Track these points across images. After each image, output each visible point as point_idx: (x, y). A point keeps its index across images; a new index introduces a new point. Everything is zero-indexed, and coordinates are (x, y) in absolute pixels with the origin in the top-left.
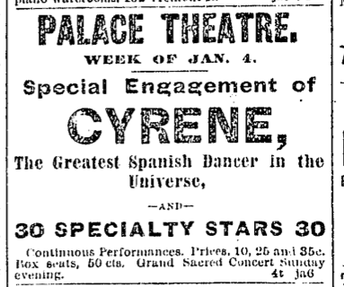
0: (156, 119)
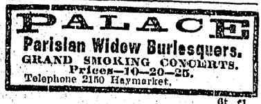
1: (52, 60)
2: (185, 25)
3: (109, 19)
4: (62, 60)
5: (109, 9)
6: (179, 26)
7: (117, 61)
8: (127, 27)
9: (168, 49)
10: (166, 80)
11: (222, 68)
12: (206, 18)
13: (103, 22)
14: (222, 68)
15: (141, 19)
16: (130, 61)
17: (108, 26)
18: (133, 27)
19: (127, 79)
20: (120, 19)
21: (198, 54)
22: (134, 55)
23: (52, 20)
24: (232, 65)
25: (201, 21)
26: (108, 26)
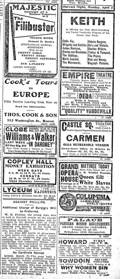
0: (82, 137)
1: (69, 227)
2: (93, 220)
3: (81, 219)
4: (71, 227)
5: (81, 217)
6: (92, 220)
7: (82, 227)
8: (84, 221)
9: (92, 197)
10: (84, 7)
11: (21, 92)
12: (96, 219)
13: (80, 220)
14: (21, 92)
15: (86, 219)
16: (85, 227)
17: (81, 221)
18: (85, 221)
19: (102, 184)
20: (83, 219)
21: (31, 25)
22: (85, 226)
23: (72, 219)
24: (106, 227)
25: (96, 219)
26: (81, 221)
